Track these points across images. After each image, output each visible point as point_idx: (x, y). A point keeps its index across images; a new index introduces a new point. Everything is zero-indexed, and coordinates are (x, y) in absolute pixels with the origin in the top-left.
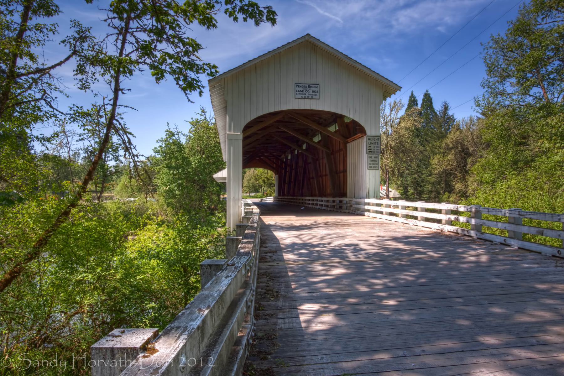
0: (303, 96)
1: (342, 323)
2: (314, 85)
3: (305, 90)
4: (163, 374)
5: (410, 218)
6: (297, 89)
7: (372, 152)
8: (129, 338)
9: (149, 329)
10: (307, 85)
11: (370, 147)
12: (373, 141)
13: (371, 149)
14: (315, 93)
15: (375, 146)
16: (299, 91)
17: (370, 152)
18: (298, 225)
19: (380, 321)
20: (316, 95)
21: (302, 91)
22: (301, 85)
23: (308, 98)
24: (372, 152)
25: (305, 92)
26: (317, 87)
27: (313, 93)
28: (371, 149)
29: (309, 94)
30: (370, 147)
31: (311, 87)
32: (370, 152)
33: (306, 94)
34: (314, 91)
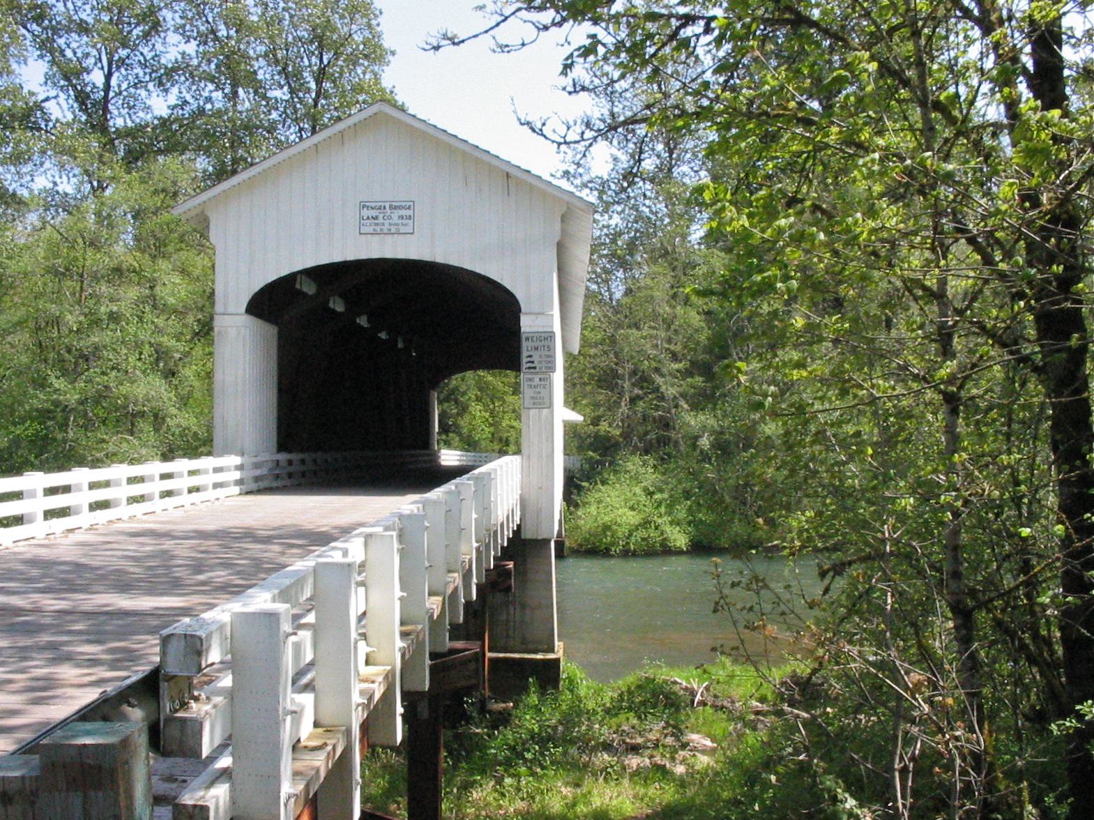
0: (378, 229)
1: (405, 594)
2: (403, 204)
3: (381, 216)
4: (1093, 634)
5: (136, 477)
6: (366, 213)
7: (535, 368)
8: (622, 532)
9: (817, 573)
10: (387, 205)
11: (530, 356)
12: (536, 344)
13: (533, 362)
14: (404, 221)
15: (543, 353)
16: (368, 218)
17: (530, 368)
18: (520, 476)
19: (229, 641)
20: (406, 225)
21: (376, 218)
22: (373, 205)
23: (389, 233)
24: (535, 368)
25: (381, 220)
26: (409, 208)
27: (400, 221)
28: (533, 362)
29: (390, 224)
30: (530, 356)
31: (396, 208)
32: (530, 368)
33: (383, 224)
34: (401, 217)
